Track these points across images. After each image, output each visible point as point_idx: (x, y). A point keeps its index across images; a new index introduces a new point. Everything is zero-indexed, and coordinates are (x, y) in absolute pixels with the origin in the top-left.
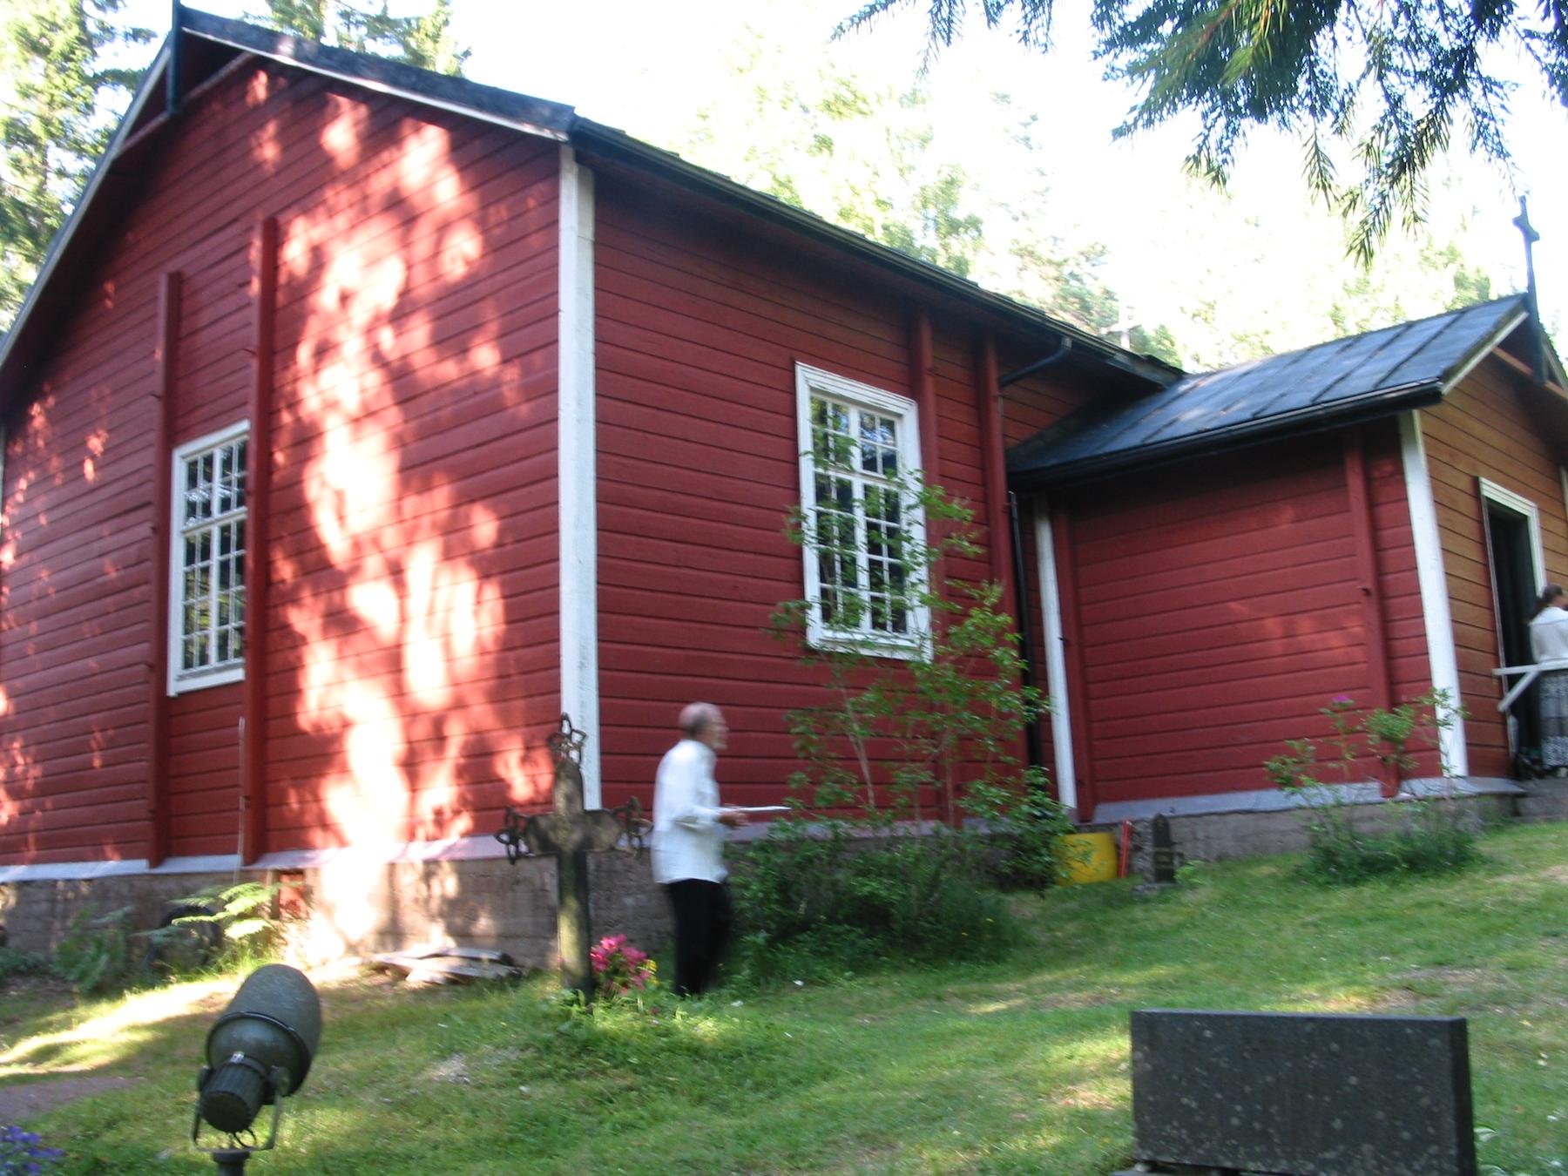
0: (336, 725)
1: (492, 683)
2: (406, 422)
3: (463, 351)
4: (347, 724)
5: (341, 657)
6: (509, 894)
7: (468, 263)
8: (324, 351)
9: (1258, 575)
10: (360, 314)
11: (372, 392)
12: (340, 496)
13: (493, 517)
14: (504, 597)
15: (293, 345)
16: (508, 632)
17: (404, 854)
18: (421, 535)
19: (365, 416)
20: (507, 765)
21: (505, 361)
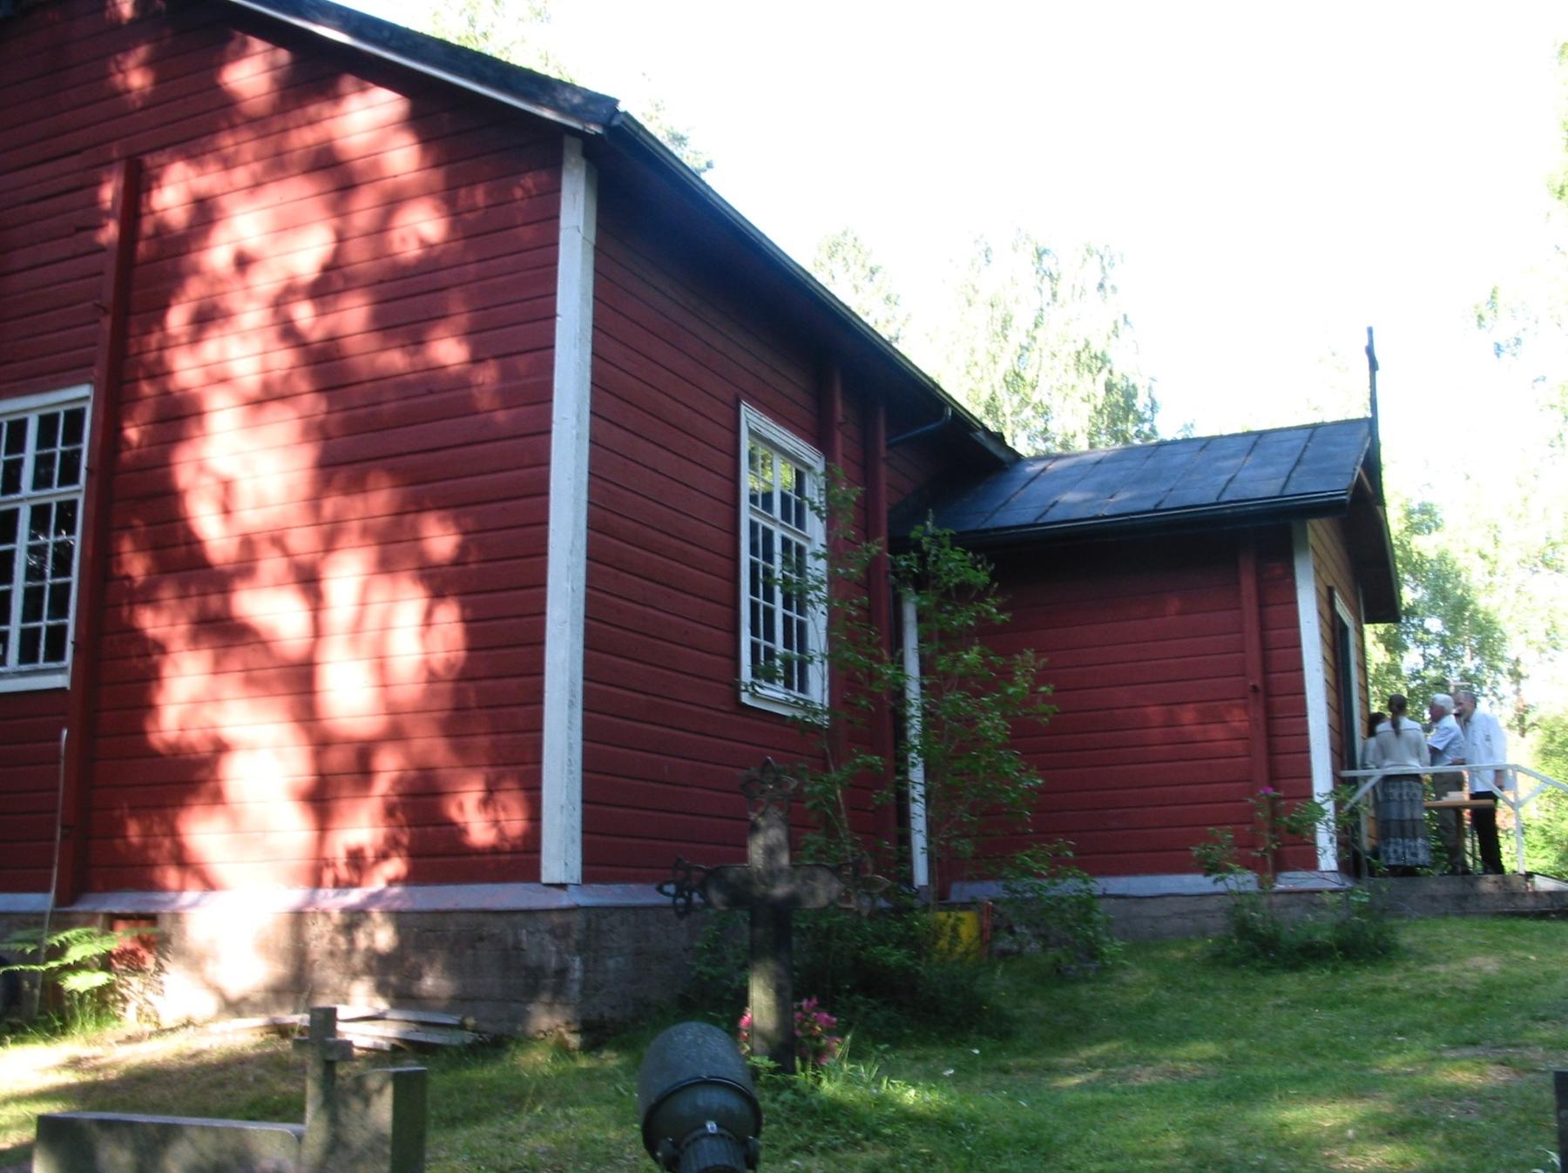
0: (205, 749)
1: (447, 714)
2: (329, 413)
3: (417, 342)
4: (222, 747)
5: (217, 669)
6: (470, 952)
7: (424, 244)
8: (207, 318)
10: (265, 281)
11: (277, 374)
12: (227, 485)
13: (453, 530)
14: (464, 620)
15: (161, 308)
16: (468, 659)
17: (311, 901)
18: (344, 541)
19: (265, 398)
20: (461, 807)
21: (476, 360)
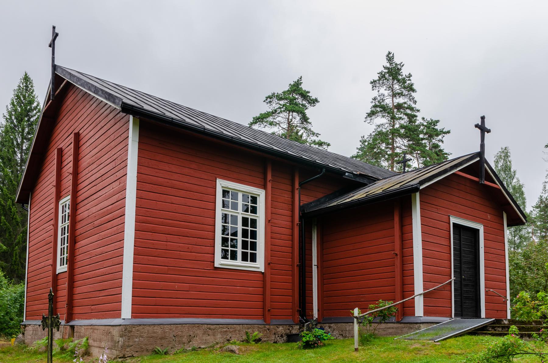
9: (367, 245)
